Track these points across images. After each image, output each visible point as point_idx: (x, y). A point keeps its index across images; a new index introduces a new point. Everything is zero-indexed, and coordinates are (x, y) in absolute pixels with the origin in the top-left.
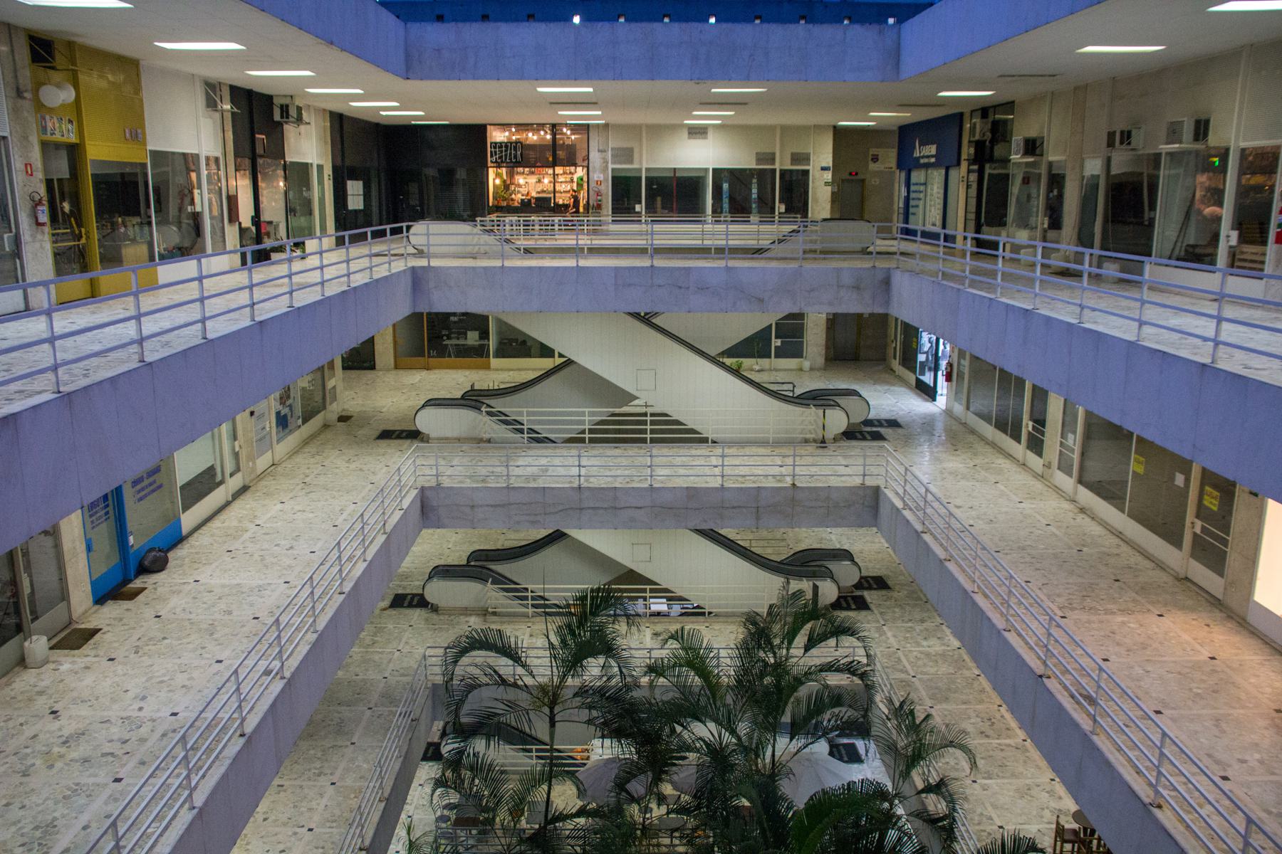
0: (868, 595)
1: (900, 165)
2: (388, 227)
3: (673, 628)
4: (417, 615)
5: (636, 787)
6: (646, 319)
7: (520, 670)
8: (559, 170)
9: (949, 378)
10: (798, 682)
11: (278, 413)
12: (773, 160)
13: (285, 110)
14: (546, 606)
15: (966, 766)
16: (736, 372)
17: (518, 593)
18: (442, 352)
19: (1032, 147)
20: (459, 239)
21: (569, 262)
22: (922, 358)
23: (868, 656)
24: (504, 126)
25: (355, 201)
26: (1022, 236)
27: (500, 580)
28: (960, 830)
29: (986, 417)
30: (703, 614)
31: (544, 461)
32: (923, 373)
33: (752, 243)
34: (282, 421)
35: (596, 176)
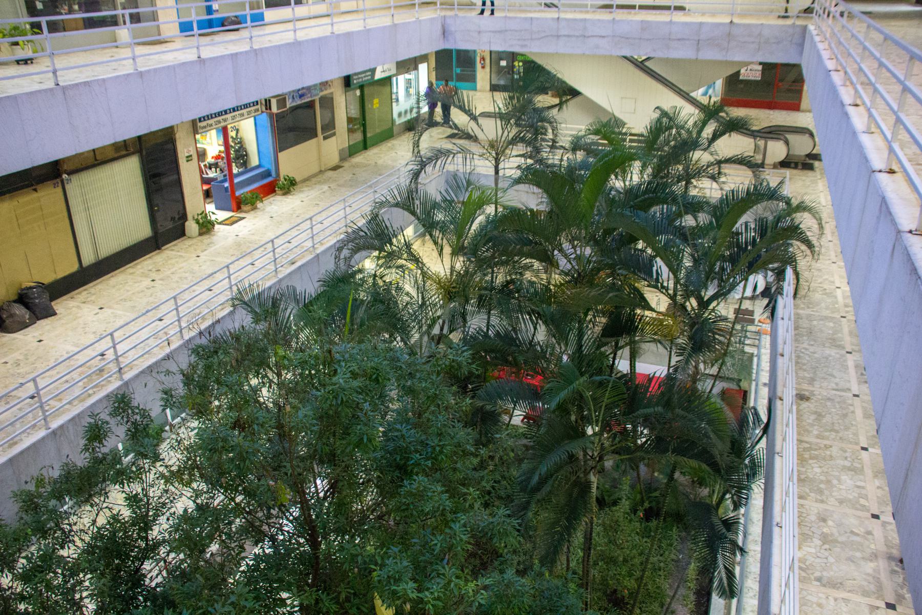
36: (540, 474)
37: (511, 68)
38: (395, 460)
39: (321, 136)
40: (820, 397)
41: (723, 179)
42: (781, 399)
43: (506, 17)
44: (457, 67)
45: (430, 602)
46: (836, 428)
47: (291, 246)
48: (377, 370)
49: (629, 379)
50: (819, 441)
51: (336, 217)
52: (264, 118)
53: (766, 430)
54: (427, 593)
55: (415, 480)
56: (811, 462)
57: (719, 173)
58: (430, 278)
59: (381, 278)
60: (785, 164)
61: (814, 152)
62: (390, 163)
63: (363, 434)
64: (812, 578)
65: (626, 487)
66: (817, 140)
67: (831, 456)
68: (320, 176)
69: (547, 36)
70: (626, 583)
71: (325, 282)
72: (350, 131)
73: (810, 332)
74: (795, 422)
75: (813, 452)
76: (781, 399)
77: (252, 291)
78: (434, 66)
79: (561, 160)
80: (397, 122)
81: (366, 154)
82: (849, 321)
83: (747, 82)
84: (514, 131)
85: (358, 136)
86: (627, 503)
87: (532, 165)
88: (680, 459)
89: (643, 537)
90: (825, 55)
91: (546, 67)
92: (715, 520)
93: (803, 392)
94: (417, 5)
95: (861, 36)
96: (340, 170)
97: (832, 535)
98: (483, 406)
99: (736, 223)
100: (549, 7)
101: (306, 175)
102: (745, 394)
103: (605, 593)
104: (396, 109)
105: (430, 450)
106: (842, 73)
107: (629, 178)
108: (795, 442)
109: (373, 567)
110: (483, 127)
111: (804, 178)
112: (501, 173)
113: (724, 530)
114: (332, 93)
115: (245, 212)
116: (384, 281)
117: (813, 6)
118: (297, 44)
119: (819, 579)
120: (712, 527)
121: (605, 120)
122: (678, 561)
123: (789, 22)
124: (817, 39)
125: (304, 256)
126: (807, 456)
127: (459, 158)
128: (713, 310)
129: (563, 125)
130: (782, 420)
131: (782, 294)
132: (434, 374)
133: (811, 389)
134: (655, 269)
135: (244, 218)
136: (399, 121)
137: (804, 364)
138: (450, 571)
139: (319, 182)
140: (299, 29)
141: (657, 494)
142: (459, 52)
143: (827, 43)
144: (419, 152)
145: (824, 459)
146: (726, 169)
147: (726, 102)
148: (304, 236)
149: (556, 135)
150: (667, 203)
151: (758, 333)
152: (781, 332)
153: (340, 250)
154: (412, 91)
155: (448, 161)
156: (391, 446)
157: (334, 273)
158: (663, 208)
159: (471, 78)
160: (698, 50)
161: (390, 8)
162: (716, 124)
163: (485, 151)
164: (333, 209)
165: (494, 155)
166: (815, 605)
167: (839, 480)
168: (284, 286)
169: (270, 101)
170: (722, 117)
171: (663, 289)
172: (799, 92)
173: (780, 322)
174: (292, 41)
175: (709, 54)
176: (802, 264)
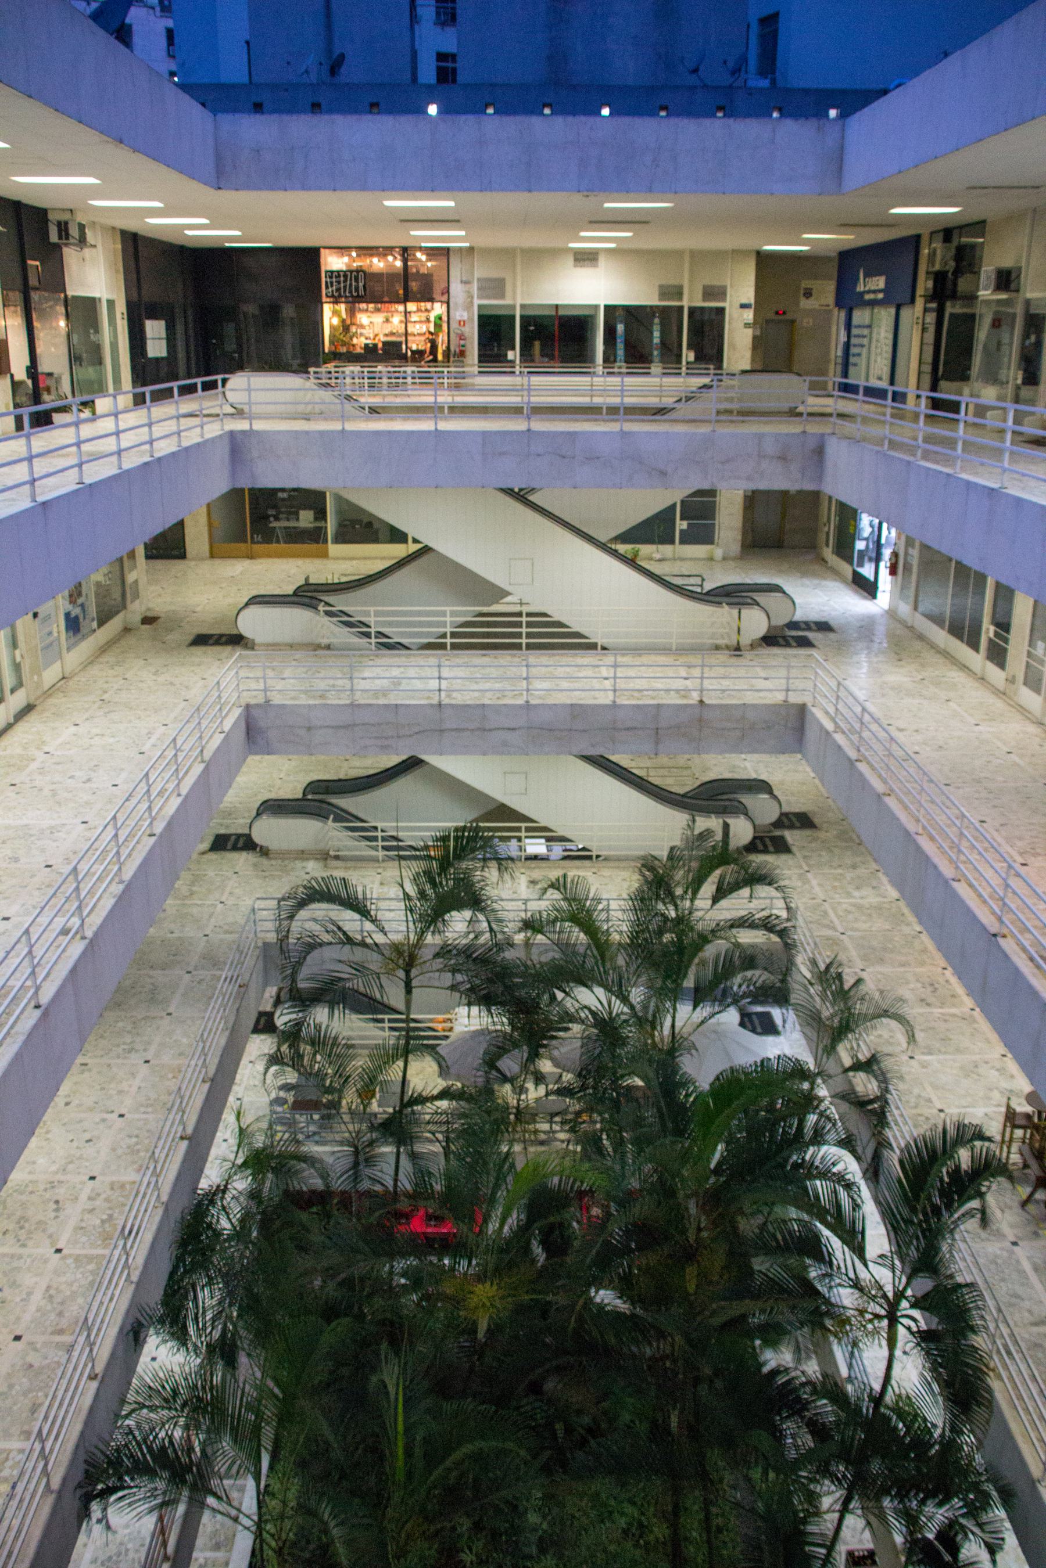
0: (790, 836)
1: (839, 303)
2: (199, 381)
3: (554, 874)
4: (242, 860)
5: (509, 1064)
6: (521, 496)
7: (368, 926)
8: (411, 306)
9: (893, 571)
10: (704, 939)
11: (67, 615)
12: (679, 294)
13: (63, 228)
14: (398, 848)
15: (901, 1038)
16: (631, 562)
17: (366, 833)
18: (268, 536)
19: (1006, 280)
20: (288, 396)
21: (425, 425)
22: (860, 545)
23: (788, 909)
24: (342, 250)
25: (156, 348)
26: (989, 394)
27: (343, 816)
28: (894, 1114)
29: (937, 620)
30: (589, 858)
31: (395, 672)
32: (861, 564)
33: (653, 401)
34: (73, 625)
35: (459, 314)
71: (130, 26)
106: (925, 837)
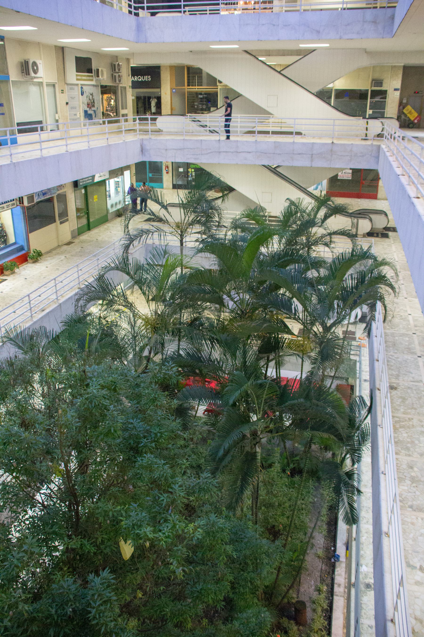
36: (224, 449)
37: (186, 174)
38: (130, 444)
39: (58, 222)
40: (403, 387)
41: (332, 245)
42: (379, 390)
43: (184, 139)
44: (150, 172)
45: (163, 539)
46: (415, 406)
47: (41, 299)
48: (115, 383)
49: (278, 380)
50: (404, 416)
51: (72, 278)
52: (18, 210)
53: (370, 410)
54: (160, 534)
55: (145, 457)
56: (400, 430)
57: (331, 241)
58: (140, 317)
59: (105, 319)
60: (370, 234)
61: (388, 226)
62: (107, 239)
63: (111, 427)
64: (407, 506)
65: (278, 455)
66: (389, 218)
67: (413, 426)
68: (58, 249)
69: (212, 152)
70: (280, 520)
72: (78, 217)
73: (394, 345)
74: (390, 405)
75: (401, 423)
76: (379, 390)
77: (16, 330)
78: (134, 172)
79: (226, 235)
80: (110, 212)
81: (89, 234)
82: (418, 336)
83: (343, 181)
84: (192, 217)
85: (84, 221)
86: (279, 465)
87: (206, 239)
88: (316, 433)
89: (290, 488)
90: (395, 165)
91: (213, 174)
92: (342, 473)
93: (392, 384)
94: (124, 132)
95: (417, 154)
96: (73, 245)
97: (417, 477)
98: (182, 404)
99: (345, 274)
100: (212, 132)
101: (48, 249)
102: (352, 388)
103: (267, 529)
104: (109, 203)
105: (153, 436)
106: (406, 177)
107: (270, 246)
108: (391, 417)
109: (121, 518)
110: (172, 214)
111: (383, 243)
112: (184, 244)
113: (347, 479)
114: (65, 192)
115: (7, 276)
116: (107, 321)
117: (382, 133)
118: (42, 159)
119: (411, 507)
120: (339, 477)
121: (253, 208)
122: (314, 503)
123: (369, 143)
124: (388, 154)
125: (50, 305)
126: (398, 426)
127: (156, 235)
128: (334, 332)
129: (225, 211)
130: (381, 403)
131: (374, 320)
132: (154, 384)
133: (398, 382)
134: (293, 307)
135: (6, 280)
136: (111, 210)
137: (392, 366)
138: (174, 517)
139: (58, 254)
140: (44, 149)
141: (297, 458)
142: (150, 163)
143: (395, 157)
144: (128, 231)
145: (409, 427)
146: (335, 238)
147: (330, 194)
148: (50, 292)
149: (220, 219)
150: (298, 263)
151: (359, 346)
152: (376, 345)
153: (78, 300)
154: (120, 189)
155: (149, 238)
156: (127, 435)
157: (72, 317)
158: (295, 266)
159: (160, 180)
160: (312, 161)
161: (106, 133)
162: (326, 209)
163: (173, 230)
164: (70, 273)
165: (180, 233)
166: (409, 524)
167: (419, 441)
168: (37, 327)
169: (22, 197)
170: (329, 204)
171: (297, 319)
172: (376, 187)
173: (375, 339)
174: (39, 157)
175: (319, 163)
176: (388, 299)
